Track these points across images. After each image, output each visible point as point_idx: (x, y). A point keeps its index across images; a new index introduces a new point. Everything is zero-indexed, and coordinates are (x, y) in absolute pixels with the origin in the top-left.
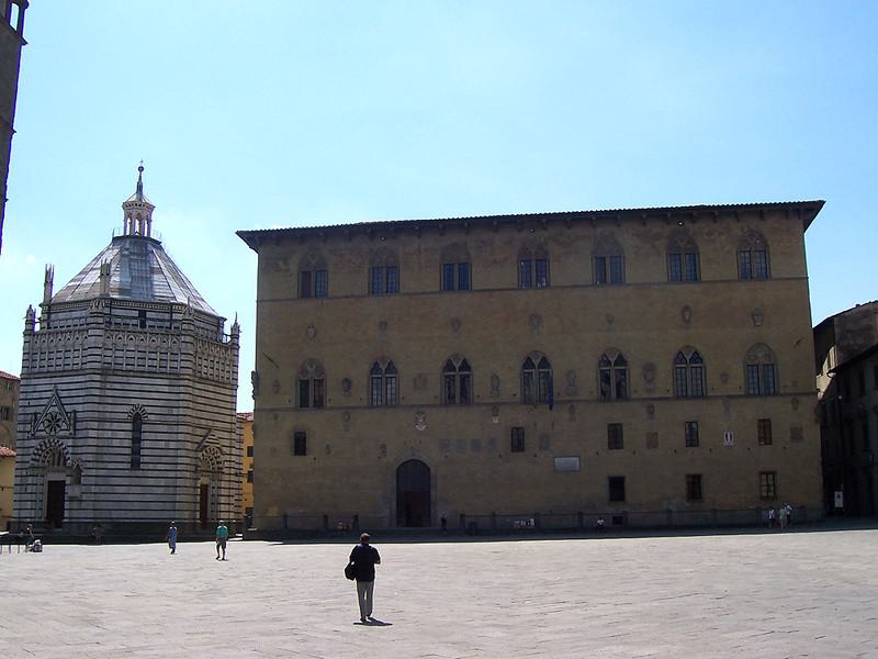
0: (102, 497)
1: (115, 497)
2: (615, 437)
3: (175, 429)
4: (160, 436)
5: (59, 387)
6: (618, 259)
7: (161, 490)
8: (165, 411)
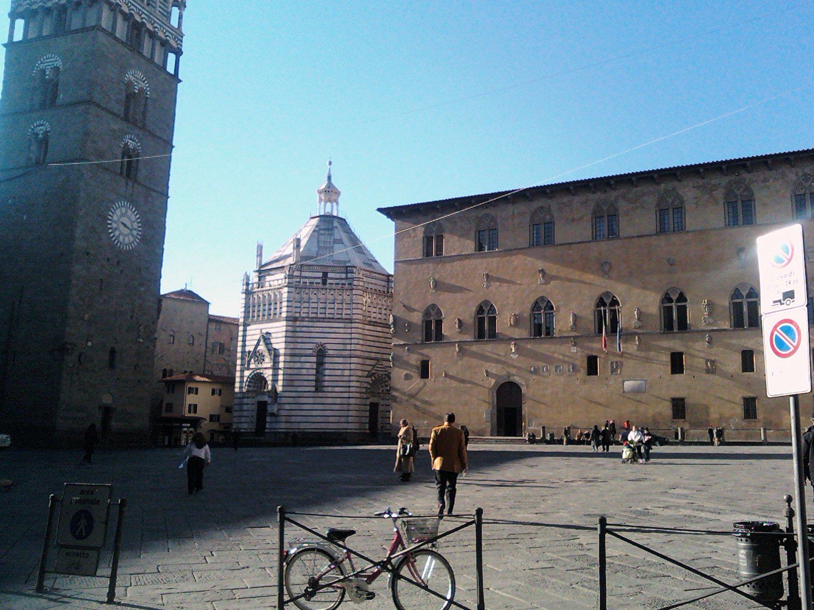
0: (294, 413)
1: (303, 413)
2: (677, 364)
3: (348, 360)
4: (336, 366)
6: (679, 210)
8: (341, 347)
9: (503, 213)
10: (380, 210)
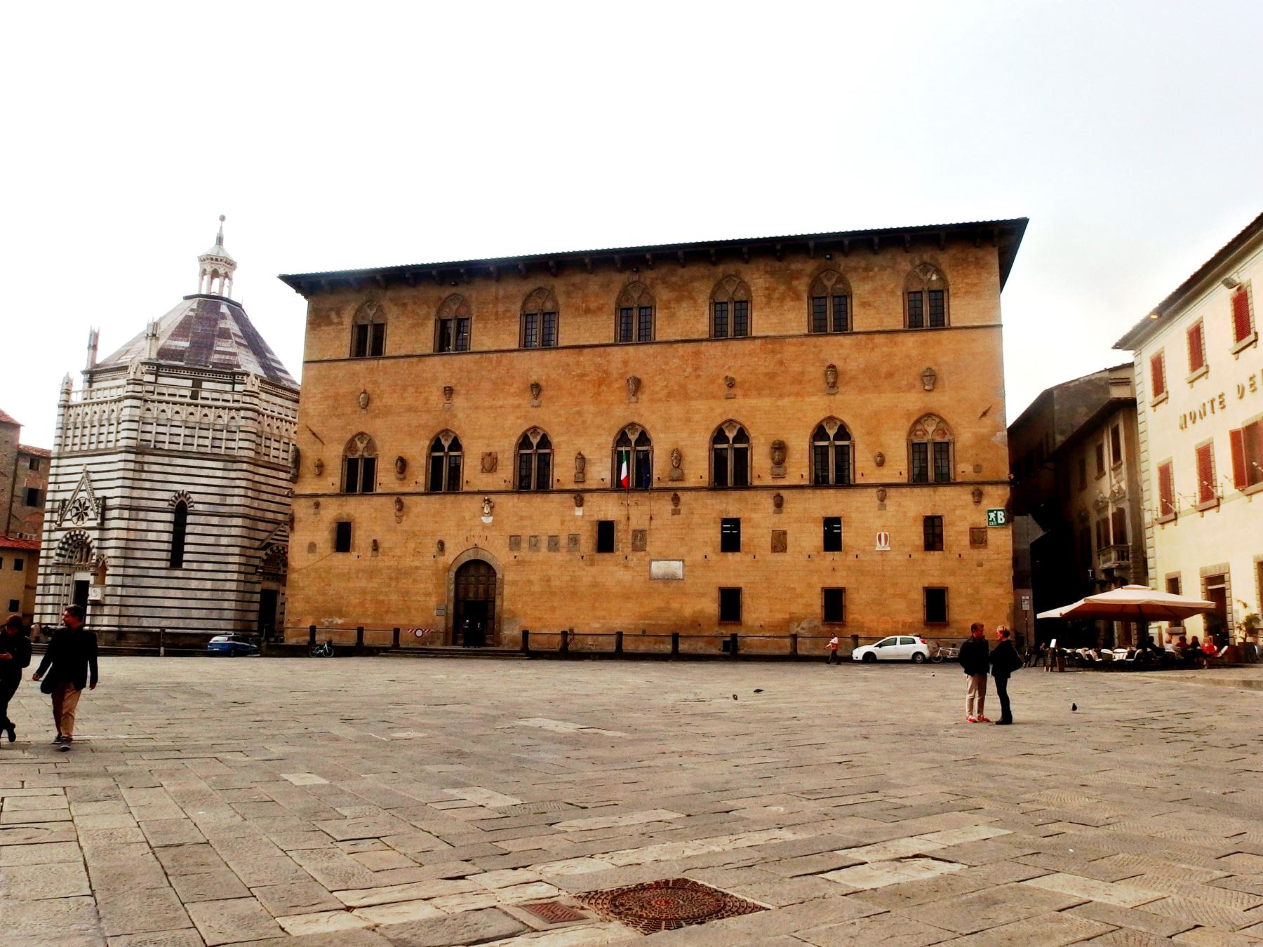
0: (132, 601)
2: (731, 539)
5: (90, 468)
7: (206, 595)
8: (216, 499)
9: (476, 294)
10: (1115, 347)
